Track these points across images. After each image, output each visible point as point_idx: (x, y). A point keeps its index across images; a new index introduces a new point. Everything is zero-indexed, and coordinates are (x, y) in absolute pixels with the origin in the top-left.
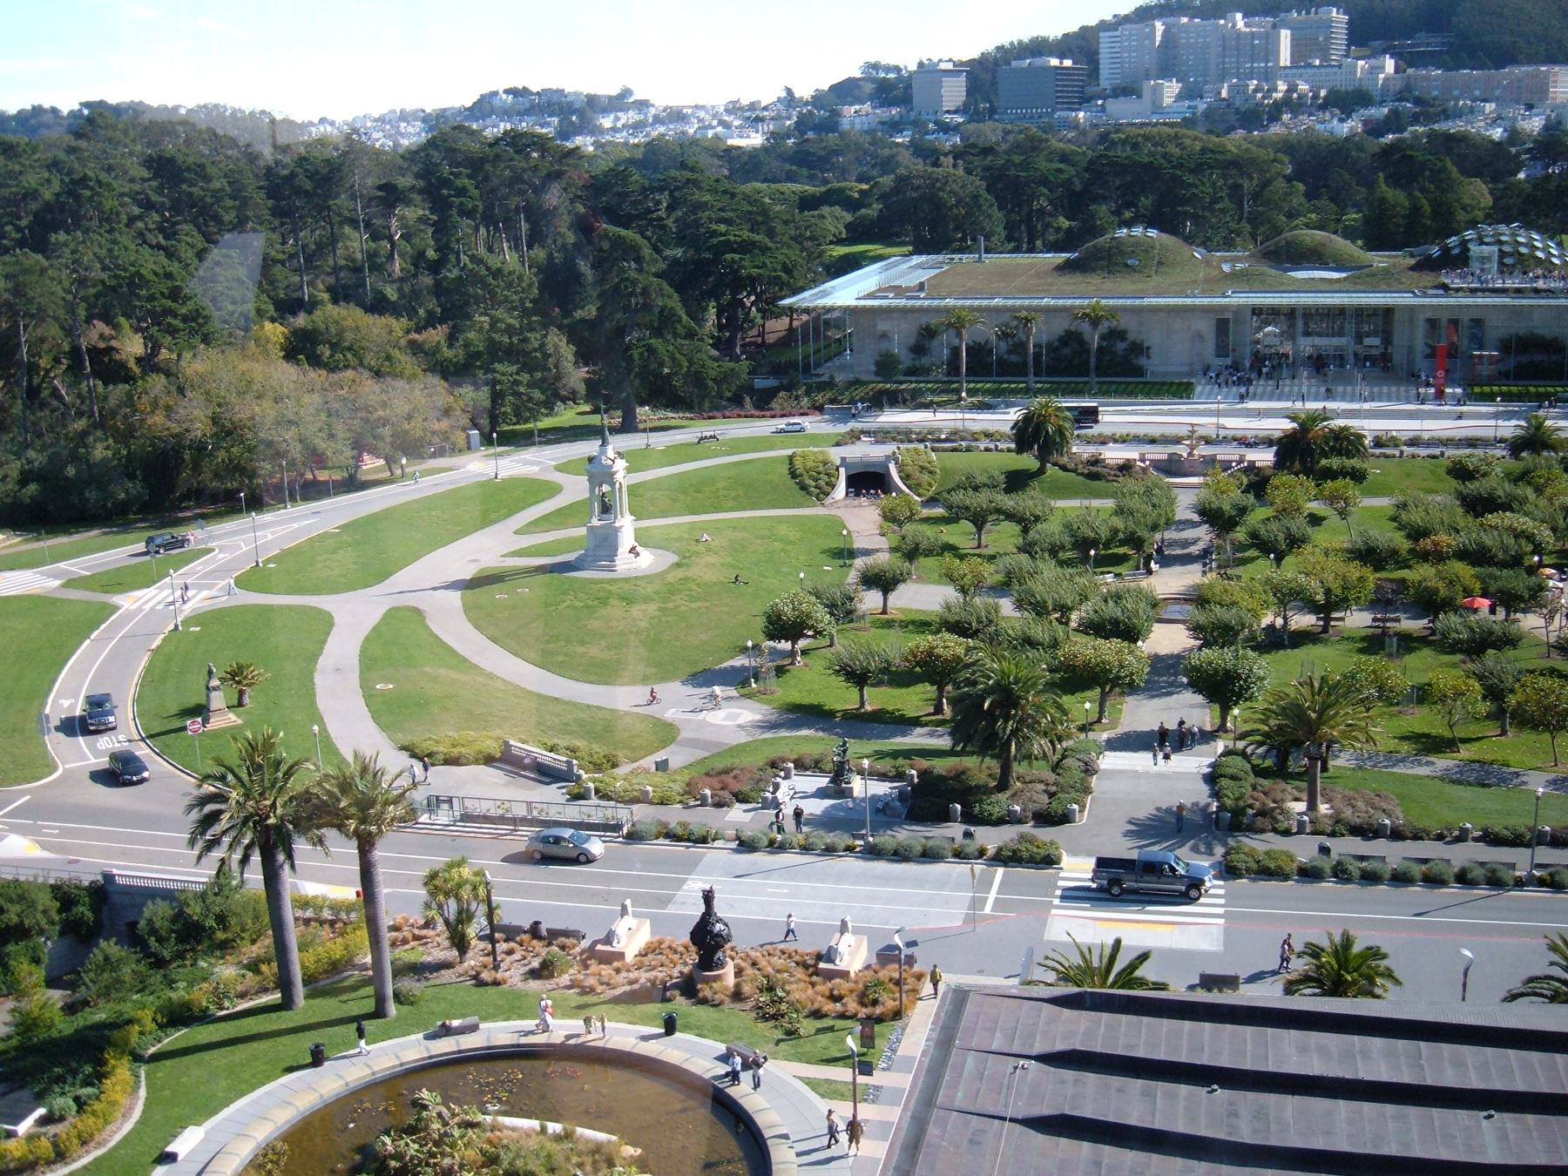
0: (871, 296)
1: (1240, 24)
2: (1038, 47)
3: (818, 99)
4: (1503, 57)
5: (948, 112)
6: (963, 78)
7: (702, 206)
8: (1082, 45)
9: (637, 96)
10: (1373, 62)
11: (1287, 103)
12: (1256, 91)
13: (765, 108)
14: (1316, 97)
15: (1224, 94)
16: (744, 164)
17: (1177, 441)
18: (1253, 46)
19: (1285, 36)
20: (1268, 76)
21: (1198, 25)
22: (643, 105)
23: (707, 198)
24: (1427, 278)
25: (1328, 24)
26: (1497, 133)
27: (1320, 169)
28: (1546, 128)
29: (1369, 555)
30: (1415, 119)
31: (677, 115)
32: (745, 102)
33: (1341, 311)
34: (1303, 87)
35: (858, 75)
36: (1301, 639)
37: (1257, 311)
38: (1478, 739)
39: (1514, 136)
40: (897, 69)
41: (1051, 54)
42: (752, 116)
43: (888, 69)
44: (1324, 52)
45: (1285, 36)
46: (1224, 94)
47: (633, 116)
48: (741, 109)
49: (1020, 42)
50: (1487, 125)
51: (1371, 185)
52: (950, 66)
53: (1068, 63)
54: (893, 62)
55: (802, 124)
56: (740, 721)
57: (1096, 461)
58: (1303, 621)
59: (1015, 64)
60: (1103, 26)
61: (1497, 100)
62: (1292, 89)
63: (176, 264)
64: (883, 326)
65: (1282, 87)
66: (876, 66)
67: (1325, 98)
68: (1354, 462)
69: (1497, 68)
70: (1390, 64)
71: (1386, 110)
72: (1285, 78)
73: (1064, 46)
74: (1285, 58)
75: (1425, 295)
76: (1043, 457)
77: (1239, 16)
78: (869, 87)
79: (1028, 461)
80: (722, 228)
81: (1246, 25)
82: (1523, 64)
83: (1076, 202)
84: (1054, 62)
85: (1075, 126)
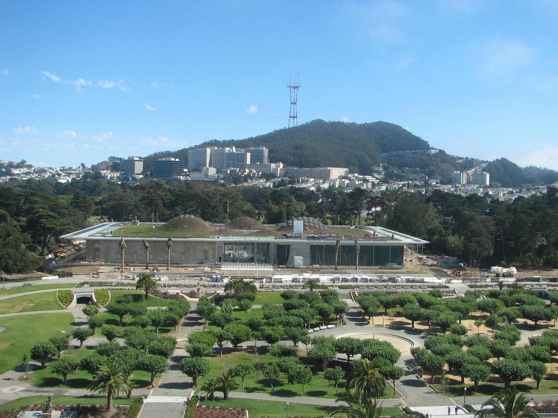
0: (90, 236)
1: (234, 150)
2: (169, 154)
3: (94, 167)
4: (317, 165)
5: (137, 174)
6: (142, 163)
7: (36, 202)
8: (183, 154)
9: (28, 163)
10: (277, 164)
11: (248, 176)
12: (239, 172)
13: (74, 170)
14: (258, 174)
15: (228, 172)
16: (61, 189)
17: (195, 286)
18: (238, 157)
19: (249, 155)
20: (243, 167)
21: (221, 150)
22: (30, 166)
23: (38, 199)
24: (280, 233)
25: (262, 152)
26: (313, 189)
27: (256, 197)
28: (330, 187)
29: (253, 326)
30: (290, 183)
31: (43, 171)
32: (67, 167)
33: (252, 244)
34: (254, 171)
35: (108, 160)
36: (228, 351)
37: (225, 243)
38: (81, 397)
39: (319, 189)
40: (121, 159)
41: (172, 157)
42: (67, 171)
43: (118, 159)
44: (261, 161)
45: (249, 155)
46: (228, 172)
47: (25, 170)
48: (66, 170)
49: (162, 152)
50: (310, 185)
51: (267, 202)
52: (138, 159)
53: (177, 160)
54: (119, 157)
55: (86, 175)
56: (16, 391)
57: (166, 294)
58: (228, 344)
59: (160, 159)
60: (191, 148)
61: (314, 178)
62: (250, 172)
63: (41, 195)
64: (97, 246)
65: (247, 171)
66: (113, 158)
67: (261, 175)
68: (250, 293)
69: (314, 167)
70: (281, 165)
71: (280, 180)
72: (249, 168)
73: (175, 155)
74: (248, 162)
75: (279, 238)
76: (147, 290)
77: (234, 148)
78: (111, 164)
79: (142, 292)
80: (41, 210)
81: (236, 151)
82: (322, 167)
83: (171, 205)
84: (173, 159)
85: (179, 181)
